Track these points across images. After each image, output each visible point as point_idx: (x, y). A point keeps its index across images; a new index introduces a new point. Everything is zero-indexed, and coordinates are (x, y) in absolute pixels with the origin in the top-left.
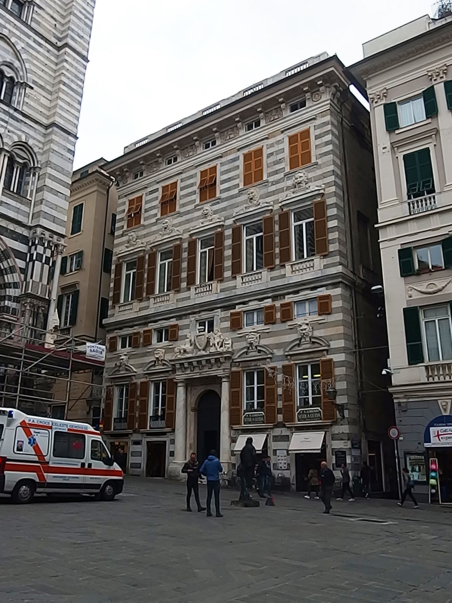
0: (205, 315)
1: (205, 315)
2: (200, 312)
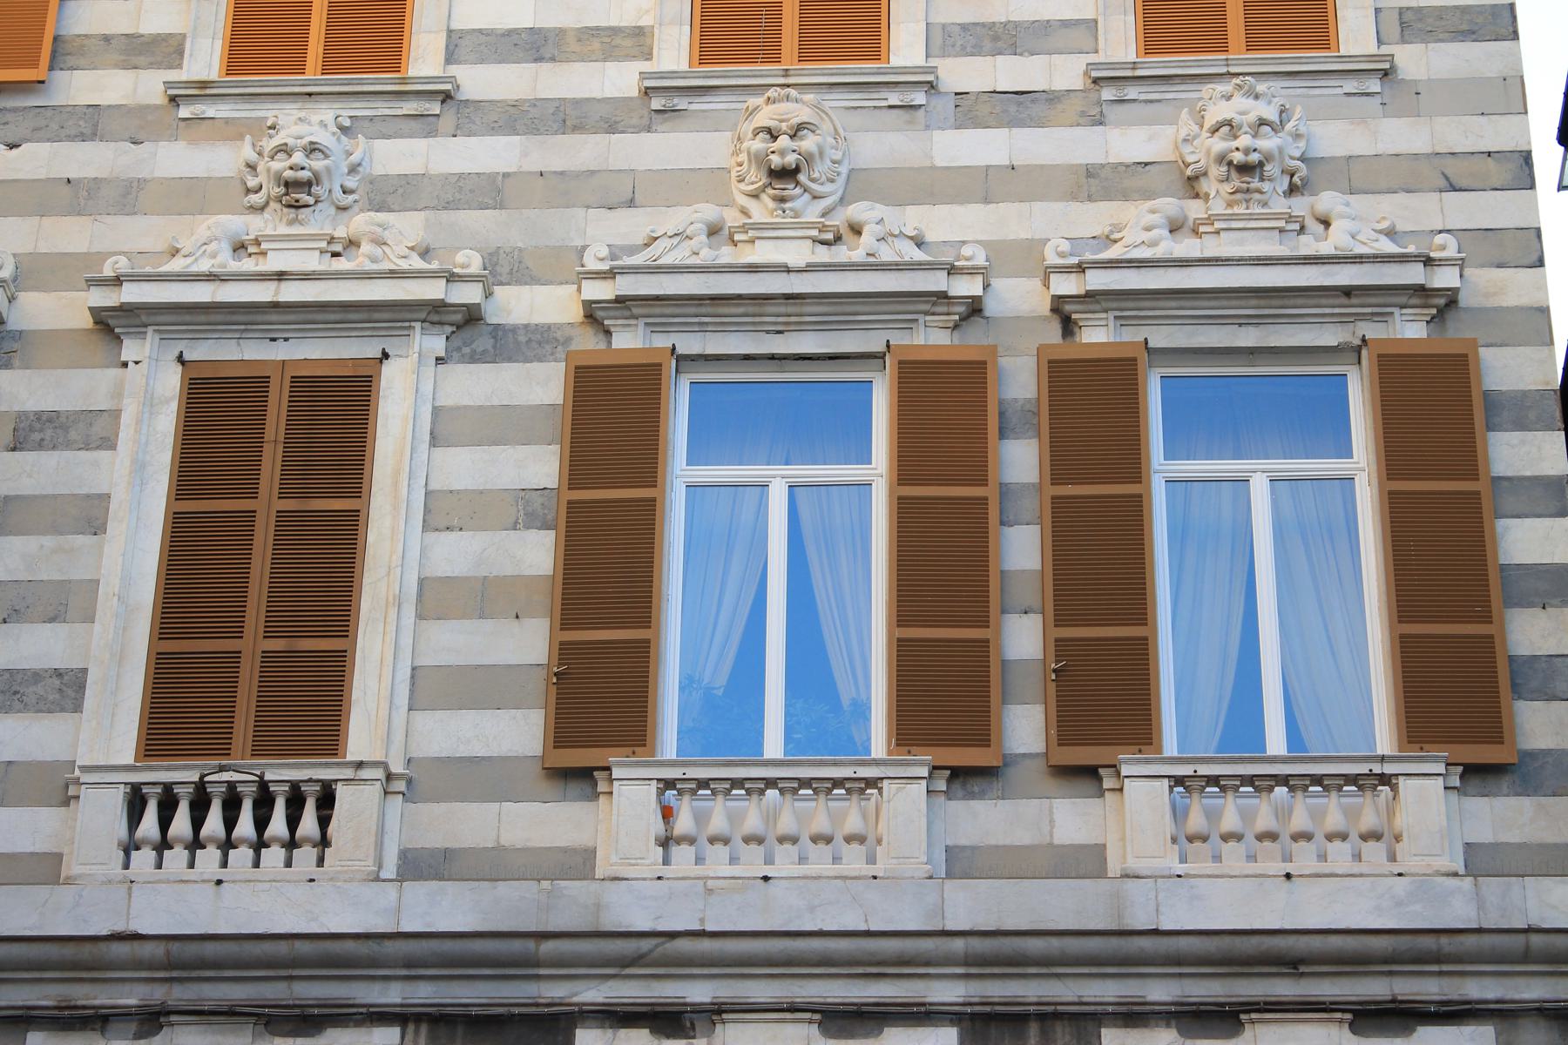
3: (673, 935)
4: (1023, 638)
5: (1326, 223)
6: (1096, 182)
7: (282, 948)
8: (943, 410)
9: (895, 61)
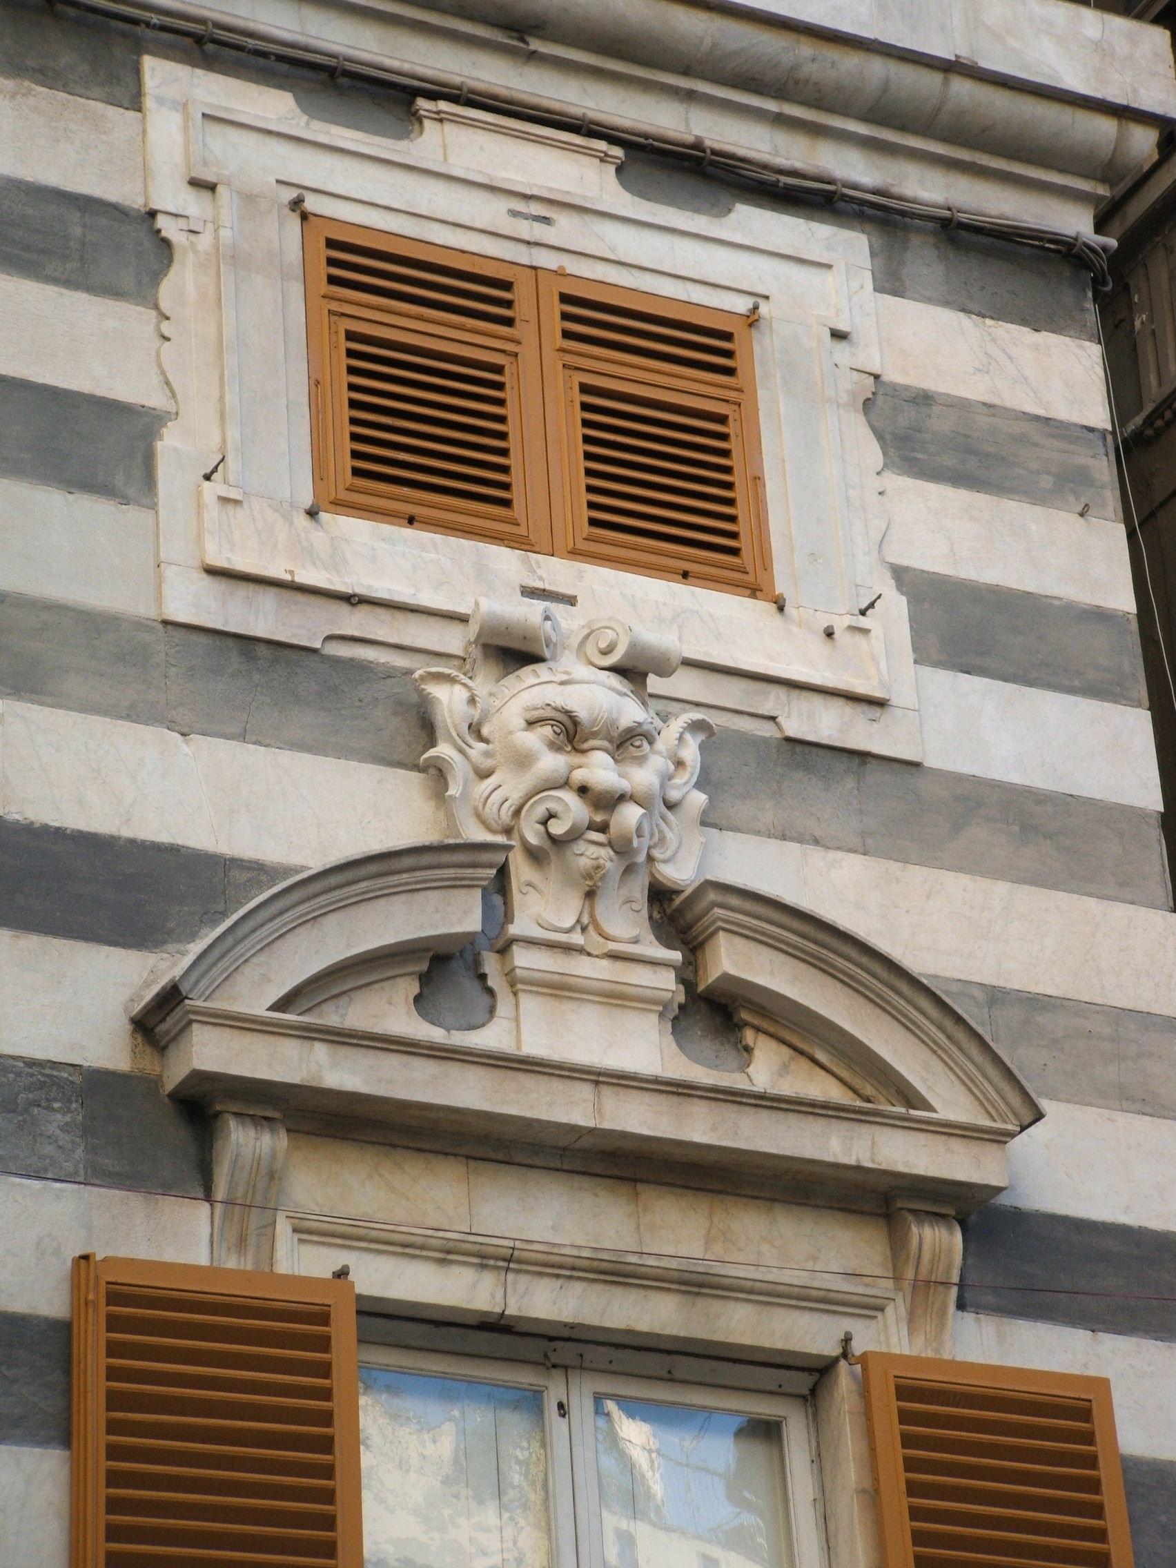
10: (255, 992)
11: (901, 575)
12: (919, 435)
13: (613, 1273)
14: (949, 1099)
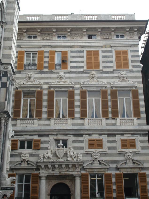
0: (60, 137)
1: (60, 137)
2: (57, 135)
3: (89, 129)
4: (110, 109)
5: (129, 81)
6: (113, 78)
7: (65, 130)
8: (104, 94)
9: (100, 69)
10: (119, 165)
11: (140, 147)
12: (141, 141)
13: (131, 171)
14: (141, 165)
